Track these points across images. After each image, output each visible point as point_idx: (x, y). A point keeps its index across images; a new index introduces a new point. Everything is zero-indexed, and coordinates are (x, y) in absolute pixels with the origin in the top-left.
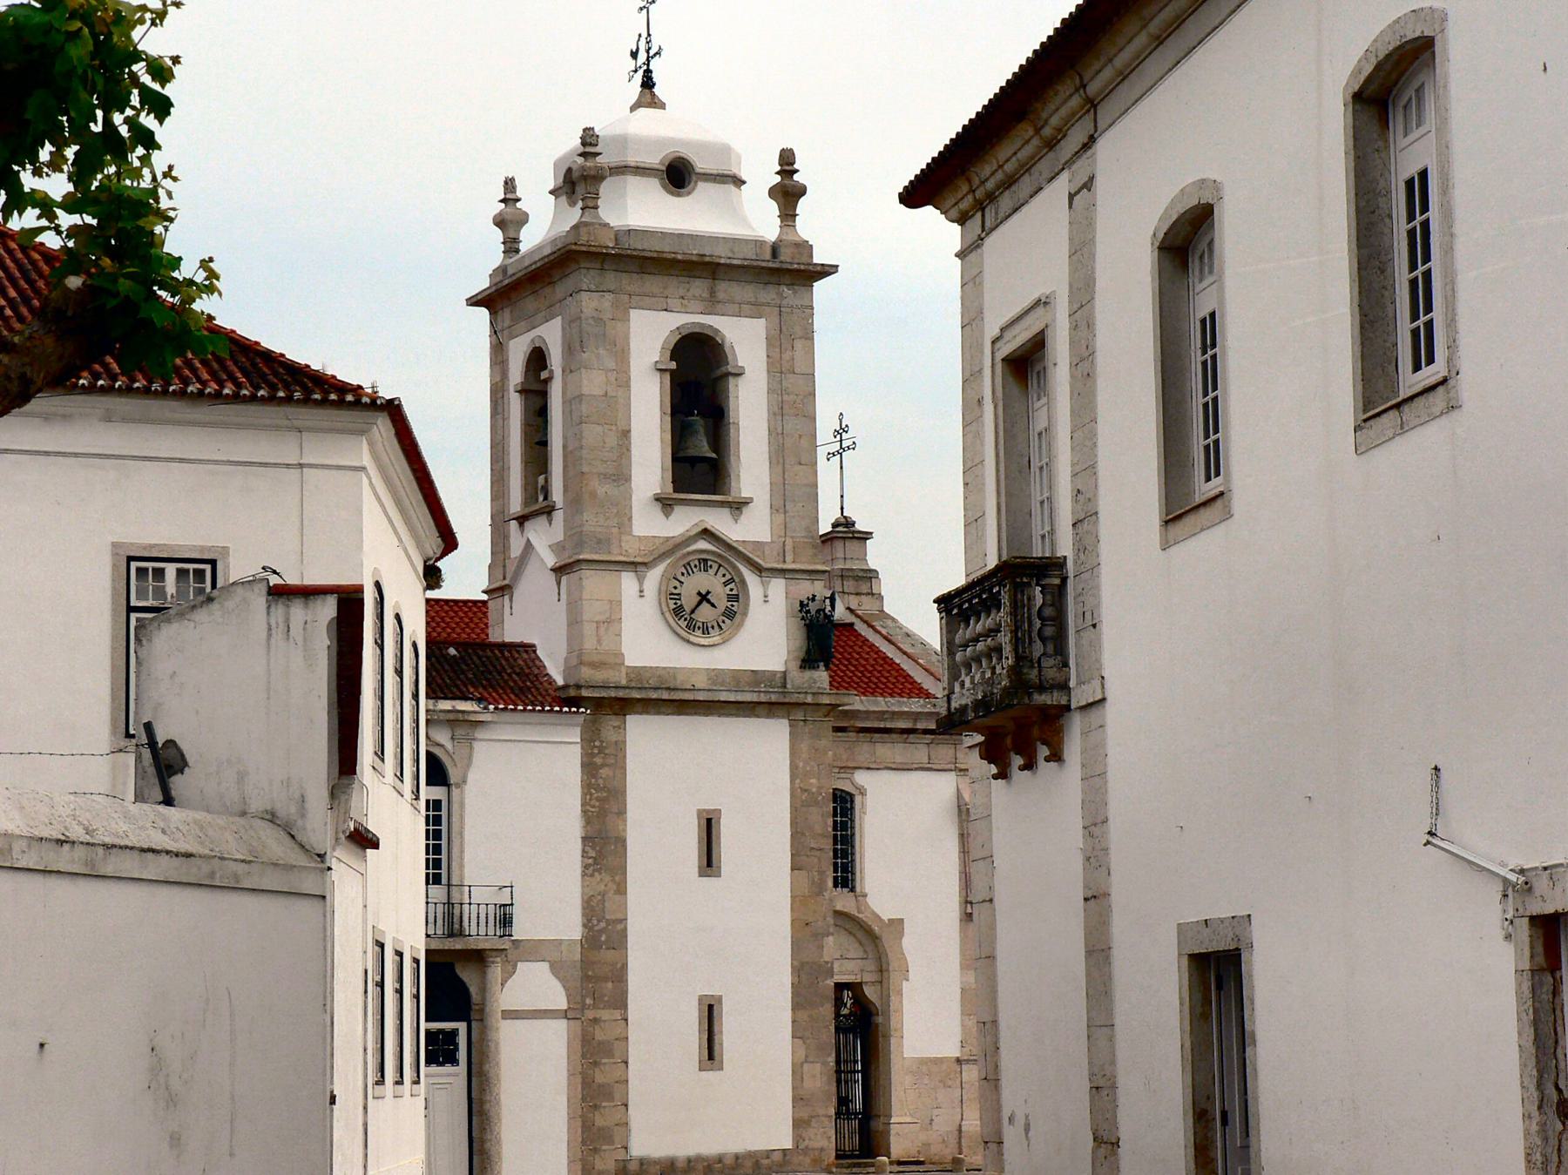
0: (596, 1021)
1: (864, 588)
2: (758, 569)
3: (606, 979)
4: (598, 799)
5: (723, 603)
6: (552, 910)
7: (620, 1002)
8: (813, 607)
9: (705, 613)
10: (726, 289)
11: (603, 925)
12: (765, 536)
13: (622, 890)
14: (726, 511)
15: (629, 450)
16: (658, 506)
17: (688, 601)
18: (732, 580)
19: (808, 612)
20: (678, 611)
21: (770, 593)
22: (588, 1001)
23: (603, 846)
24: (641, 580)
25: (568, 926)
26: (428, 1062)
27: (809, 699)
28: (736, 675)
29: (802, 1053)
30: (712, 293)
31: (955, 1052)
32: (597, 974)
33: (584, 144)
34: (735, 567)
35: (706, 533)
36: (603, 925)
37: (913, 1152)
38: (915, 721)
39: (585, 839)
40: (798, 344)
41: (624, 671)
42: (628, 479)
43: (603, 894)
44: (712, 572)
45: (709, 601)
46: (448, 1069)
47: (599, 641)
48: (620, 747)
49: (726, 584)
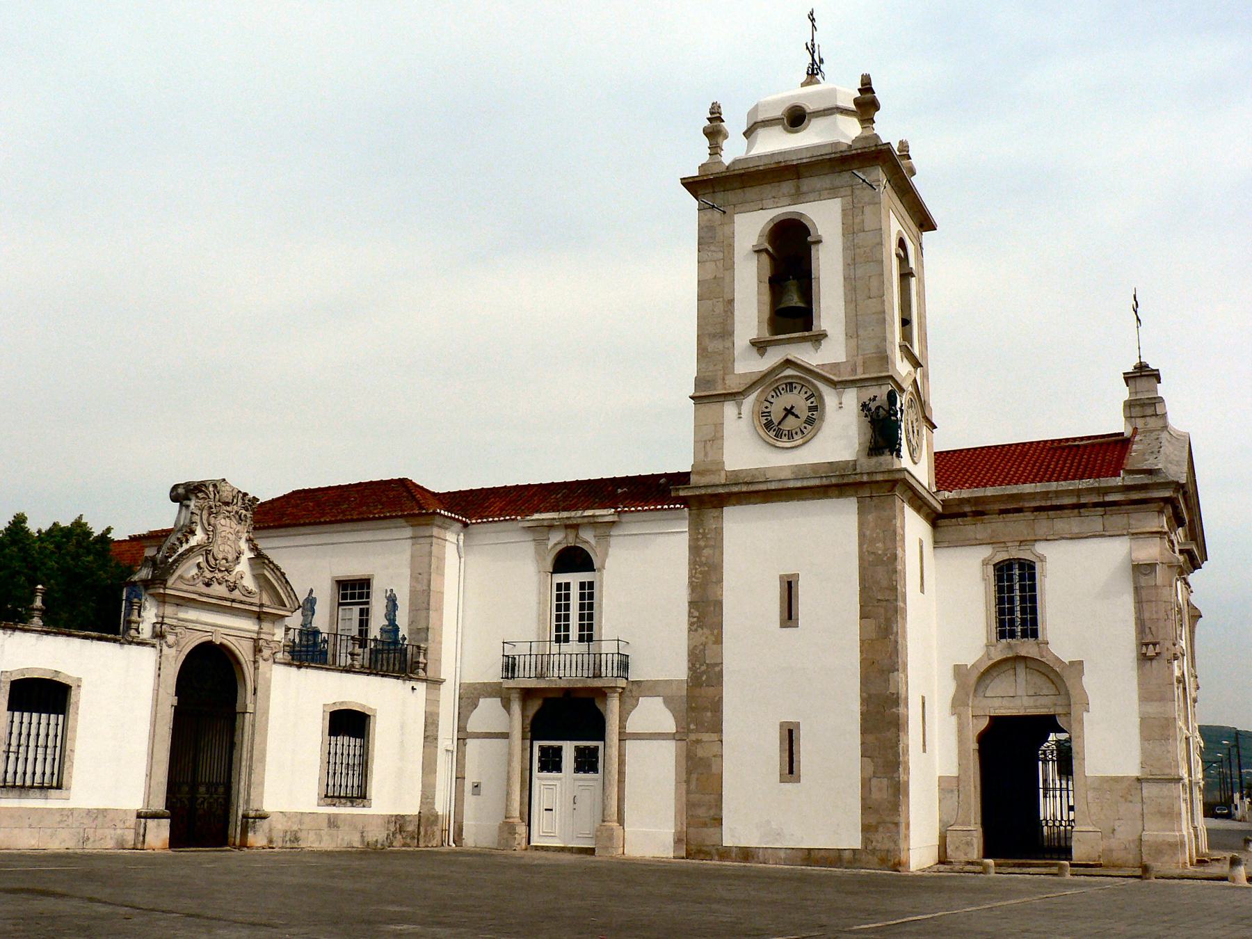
0: (698, 741)
1: (1149, 411)
2: (833, 384)
3: (705, 709)
4: (701, 573)
5: (804, 414)
6: (661, 654)
7: (717, 727)
8: (873, 406)
9: (791, 423)
10: (806, 184)
11: (704, 668)
12: (841, 358)
13: (719, 640)
14: (809, 344)
15: (733, 313)
16: (755, 350)
17: (776, 412)
18: (812, 395)
19: (870, 410)
20: (768, 425)
21: (844, 400)
22: (692, 727)
23: (705, 609)
24: (739, 405)
25: (678, 670)
26: (542, 769)
27: (865, 478)
28: (815, 467)
29: (870, 769)
30: (798, 188)
31: (1134, 771)
32: (700, 704)
33: (711, 113)
34: (814, 385)
35: (788, 363)
36: (704, 668)
37: (1095, 856)
38: (1079, 496)
39: (692, 604)
40: (868, 209)
41: (723, 474)
42: (731, 334)
43: (704, 645)
44: (796, 391)
45: (793, 414)
46: (591, 775)
47: (706, 455)
48: (719, 532)
49: (807, 399)
